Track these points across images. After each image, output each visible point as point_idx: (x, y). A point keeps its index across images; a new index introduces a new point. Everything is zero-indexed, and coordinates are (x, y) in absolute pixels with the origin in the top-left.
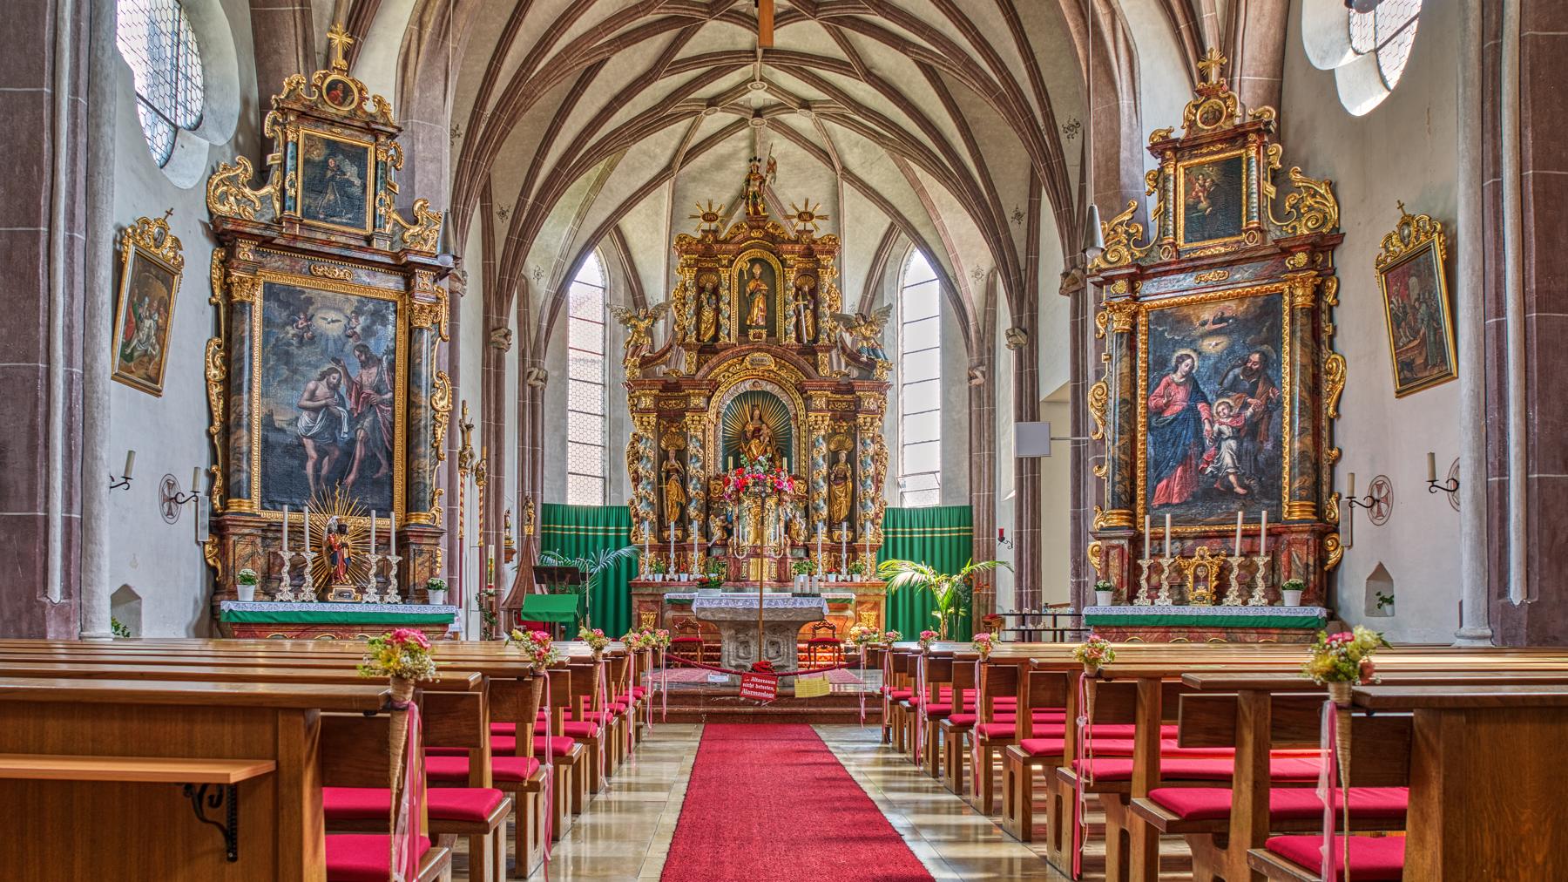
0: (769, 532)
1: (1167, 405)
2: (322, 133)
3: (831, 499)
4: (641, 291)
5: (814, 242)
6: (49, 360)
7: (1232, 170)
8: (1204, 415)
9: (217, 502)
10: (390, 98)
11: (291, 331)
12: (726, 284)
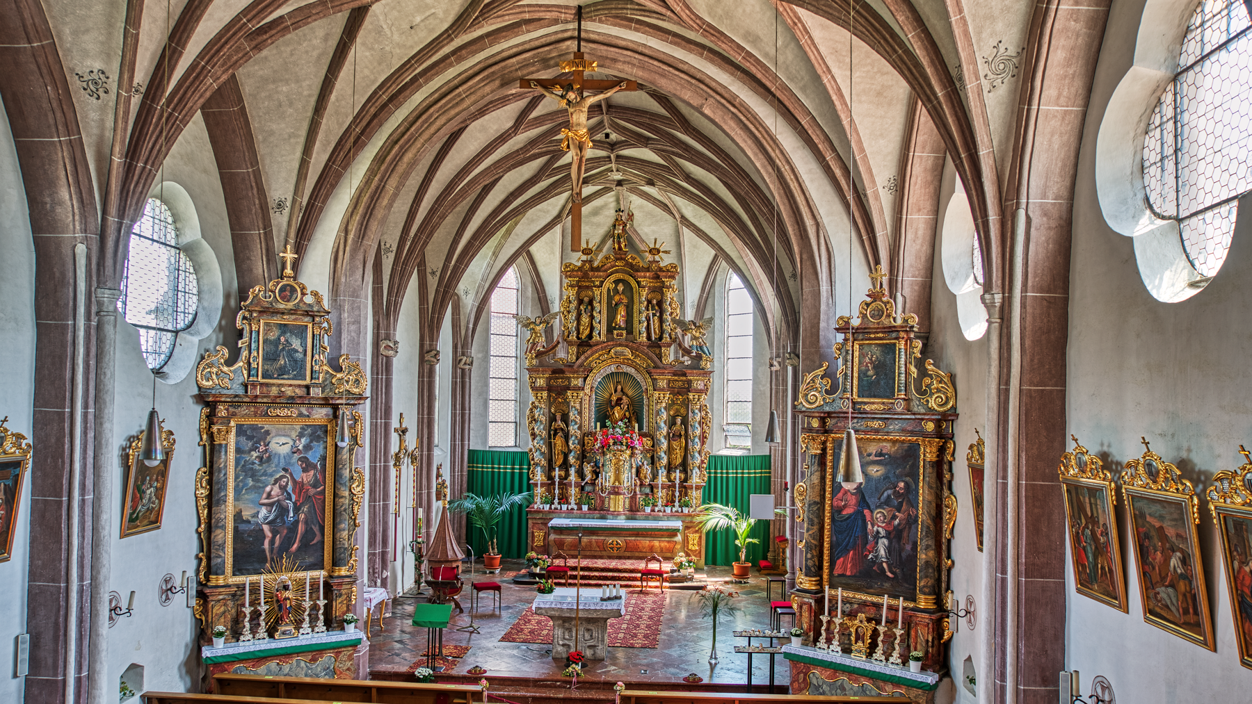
0: (625, 476)
1: (845, 506)
2: (277, 320)
3: (670, 450)
4: (544, 291)
5: (661, 269)
6: (67, 581)
7: (890, 349)
8: (868, 517)
9: (202, 576)
10: (325, 293)
11: (255, 454)
12: (598, 299)
